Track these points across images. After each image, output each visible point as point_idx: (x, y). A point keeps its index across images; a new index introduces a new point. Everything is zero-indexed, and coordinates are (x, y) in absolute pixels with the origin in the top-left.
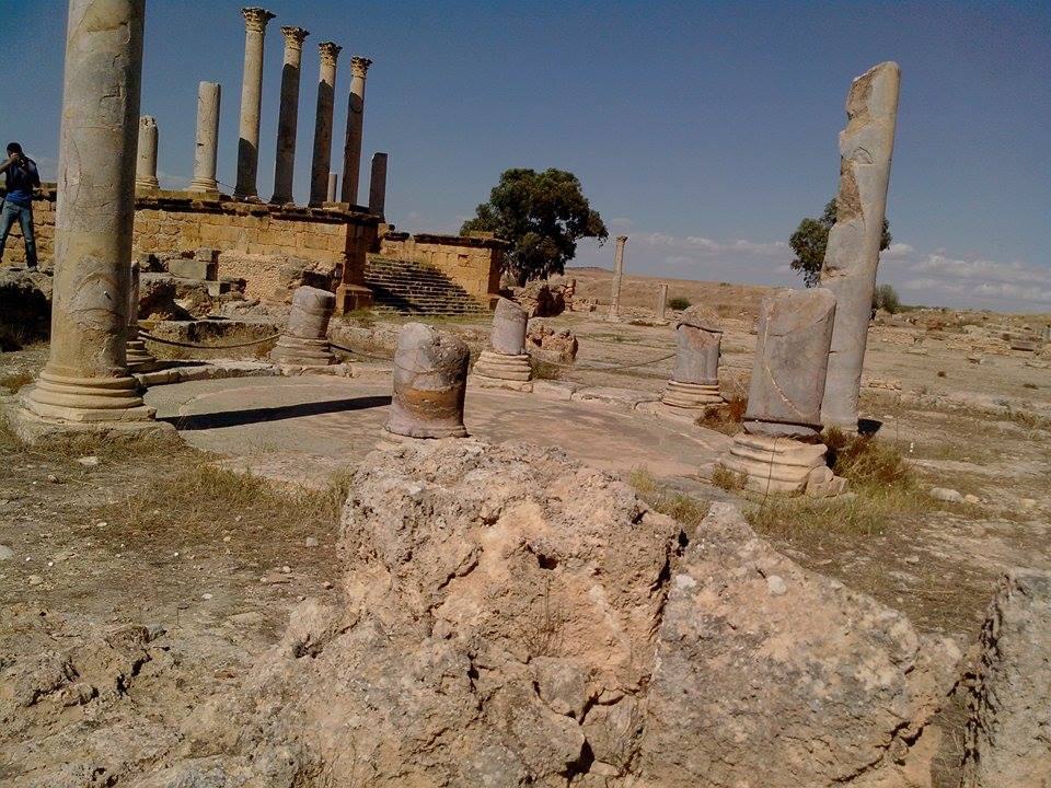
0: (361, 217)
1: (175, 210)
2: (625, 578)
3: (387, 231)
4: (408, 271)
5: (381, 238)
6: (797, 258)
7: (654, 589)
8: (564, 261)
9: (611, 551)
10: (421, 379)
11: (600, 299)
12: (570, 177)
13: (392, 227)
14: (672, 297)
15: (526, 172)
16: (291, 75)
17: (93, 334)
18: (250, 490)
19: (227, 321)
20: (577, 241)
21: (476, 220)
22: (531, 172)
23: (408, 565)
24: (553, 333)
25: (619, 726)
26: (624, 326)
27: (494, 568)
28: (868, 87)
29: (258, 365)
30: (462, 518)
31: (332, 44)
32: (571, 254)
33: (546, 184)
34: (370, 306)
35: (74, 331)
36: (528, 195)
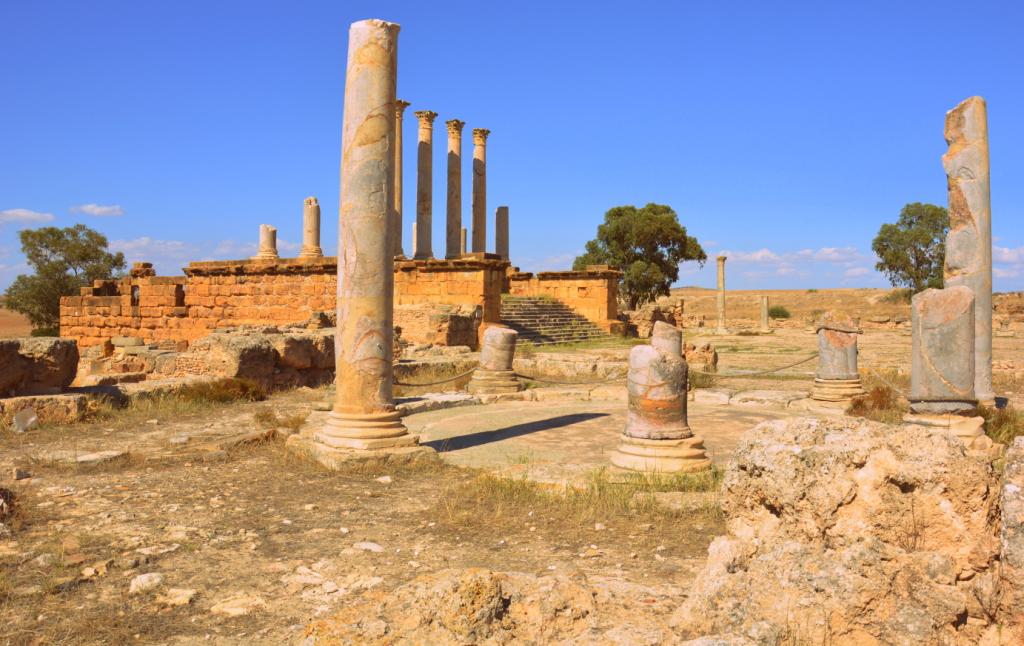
0: (495, 263)
2: (965, 492)
4: (536, 306)
5: (509, 279)
6: (880, 260)
7: (984, 499)
8: (669, 284)
9: (953, 475)
10: (654, 391)
11: (707, 314)
12: (668, 210)
13: (517, 269)
14: (774, 304)
18: (521, 494)
19: (416, 363)
21: (586, 256)
22: (633, 209)
23: (804, 502)
24: (694, 348)
25: (985, 589)
26: (734, 337)
27: (870, 498)
28: (961, 118)
29: (462, 396)
30: (840, 465)
31: (457, 121)
32: (674, 278)
35: (357, 376)
36: (631, 228)
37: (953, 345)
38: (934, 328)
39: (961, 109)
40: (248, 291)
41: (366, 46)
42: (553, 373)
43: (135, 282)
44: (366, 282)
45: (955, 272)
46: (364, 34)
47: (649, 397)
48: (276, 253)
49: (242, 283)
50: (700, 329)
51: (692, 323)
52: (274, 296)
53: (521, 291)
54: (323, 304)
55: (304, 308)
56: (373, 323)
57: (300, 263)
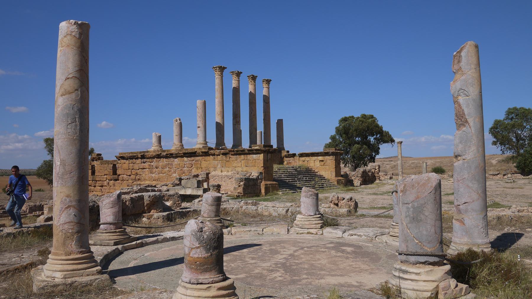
0: (269, 150)
1: (191, 157)
3: (286, 153)
5: (284, 157)
8: (375, 156)
10: (194, 251)
12: (372, 117)
13: (288, 152)
15: (350, 117)
16: (236, 92)
17: (69, 234)
20: (380, 146)
21: (330, 143)
22: (353, 117)
24: (344, 199)
28: (460, 56)
32: (377, 153)
33: (360, 121)
34: (277, 190)
35: (60, 234)
37: (422, 216)
38: (409, 204)
39: (460, 52)
40: (147, 167)
41: (65, 37)
42: (267, 214)
43: (93, 163)
44: (66, 177)
45: (459, 158)
46: (65, 27)
47: (191, 255)
48: (161, 147)
49: (144, 163)
50: (389, 181)
51: (386, 177)
52: (160, 169)
53: (290, 163)
54: (184, 173)
55: (174, 175)
56: (71, 201)
57: (173, 152)
